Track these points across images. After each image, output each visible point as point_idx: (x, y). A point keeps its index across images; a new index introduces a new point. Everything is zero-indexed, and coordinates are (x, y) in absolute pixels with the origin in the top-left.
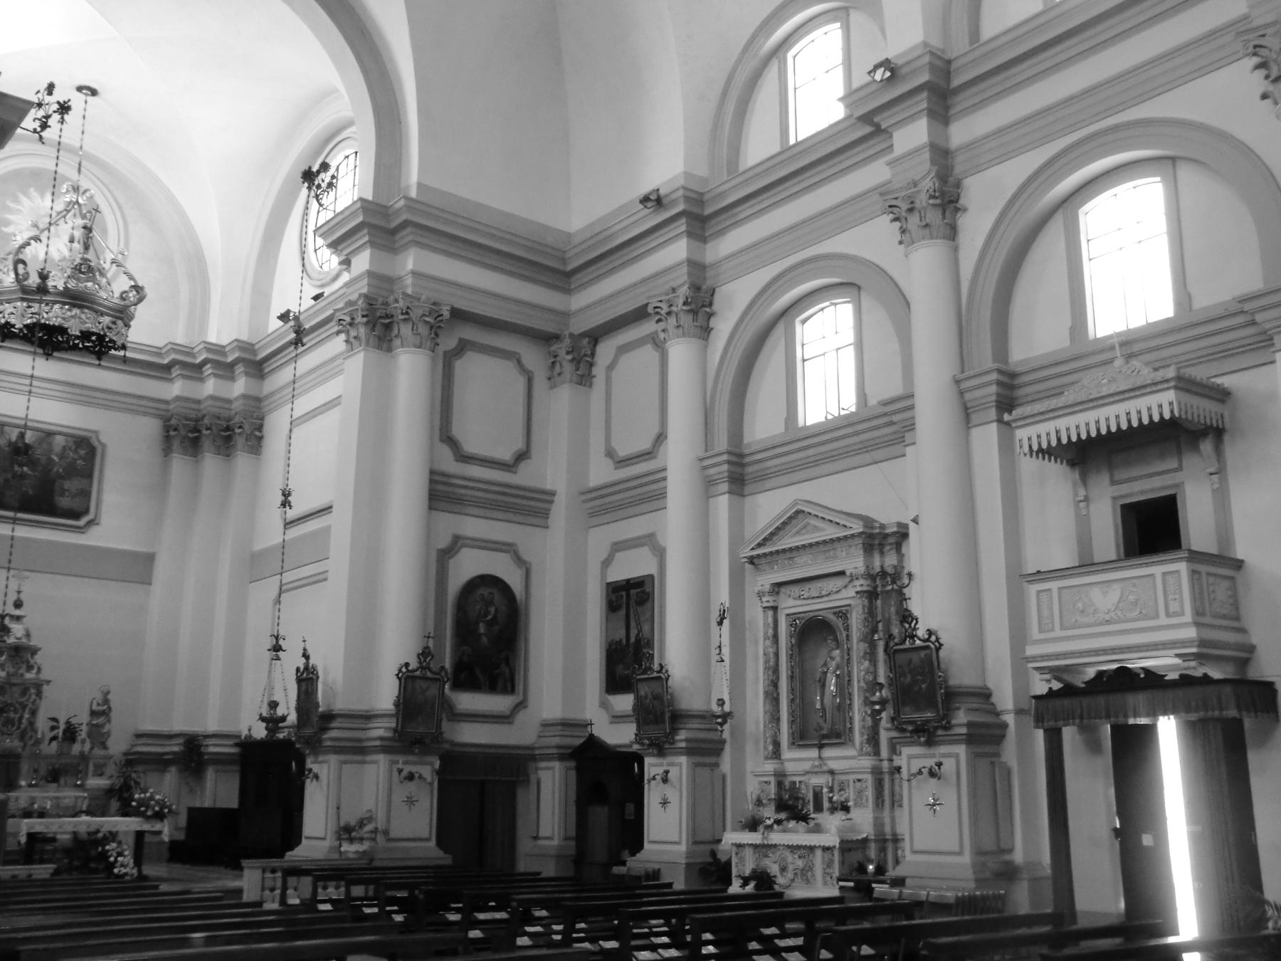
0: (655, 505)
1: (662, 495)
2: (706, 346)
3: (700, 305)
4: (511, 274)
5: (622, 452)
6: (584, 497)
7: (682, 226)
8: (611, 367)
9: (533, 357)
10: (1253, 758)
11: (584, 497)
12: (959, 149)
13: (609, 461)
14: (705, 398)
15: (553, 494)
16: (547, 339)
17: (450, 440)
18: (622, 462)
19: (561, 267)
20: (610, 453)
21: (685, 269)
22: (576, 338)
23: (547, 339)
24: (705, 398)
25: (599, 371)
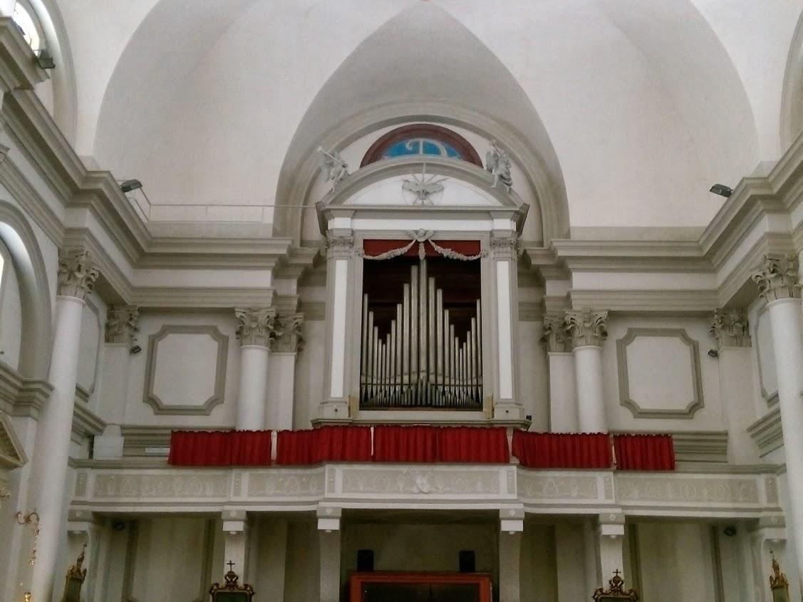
2: (574, 356)
7: (760, 206)
9: (698, 333)
17: (628, 404)
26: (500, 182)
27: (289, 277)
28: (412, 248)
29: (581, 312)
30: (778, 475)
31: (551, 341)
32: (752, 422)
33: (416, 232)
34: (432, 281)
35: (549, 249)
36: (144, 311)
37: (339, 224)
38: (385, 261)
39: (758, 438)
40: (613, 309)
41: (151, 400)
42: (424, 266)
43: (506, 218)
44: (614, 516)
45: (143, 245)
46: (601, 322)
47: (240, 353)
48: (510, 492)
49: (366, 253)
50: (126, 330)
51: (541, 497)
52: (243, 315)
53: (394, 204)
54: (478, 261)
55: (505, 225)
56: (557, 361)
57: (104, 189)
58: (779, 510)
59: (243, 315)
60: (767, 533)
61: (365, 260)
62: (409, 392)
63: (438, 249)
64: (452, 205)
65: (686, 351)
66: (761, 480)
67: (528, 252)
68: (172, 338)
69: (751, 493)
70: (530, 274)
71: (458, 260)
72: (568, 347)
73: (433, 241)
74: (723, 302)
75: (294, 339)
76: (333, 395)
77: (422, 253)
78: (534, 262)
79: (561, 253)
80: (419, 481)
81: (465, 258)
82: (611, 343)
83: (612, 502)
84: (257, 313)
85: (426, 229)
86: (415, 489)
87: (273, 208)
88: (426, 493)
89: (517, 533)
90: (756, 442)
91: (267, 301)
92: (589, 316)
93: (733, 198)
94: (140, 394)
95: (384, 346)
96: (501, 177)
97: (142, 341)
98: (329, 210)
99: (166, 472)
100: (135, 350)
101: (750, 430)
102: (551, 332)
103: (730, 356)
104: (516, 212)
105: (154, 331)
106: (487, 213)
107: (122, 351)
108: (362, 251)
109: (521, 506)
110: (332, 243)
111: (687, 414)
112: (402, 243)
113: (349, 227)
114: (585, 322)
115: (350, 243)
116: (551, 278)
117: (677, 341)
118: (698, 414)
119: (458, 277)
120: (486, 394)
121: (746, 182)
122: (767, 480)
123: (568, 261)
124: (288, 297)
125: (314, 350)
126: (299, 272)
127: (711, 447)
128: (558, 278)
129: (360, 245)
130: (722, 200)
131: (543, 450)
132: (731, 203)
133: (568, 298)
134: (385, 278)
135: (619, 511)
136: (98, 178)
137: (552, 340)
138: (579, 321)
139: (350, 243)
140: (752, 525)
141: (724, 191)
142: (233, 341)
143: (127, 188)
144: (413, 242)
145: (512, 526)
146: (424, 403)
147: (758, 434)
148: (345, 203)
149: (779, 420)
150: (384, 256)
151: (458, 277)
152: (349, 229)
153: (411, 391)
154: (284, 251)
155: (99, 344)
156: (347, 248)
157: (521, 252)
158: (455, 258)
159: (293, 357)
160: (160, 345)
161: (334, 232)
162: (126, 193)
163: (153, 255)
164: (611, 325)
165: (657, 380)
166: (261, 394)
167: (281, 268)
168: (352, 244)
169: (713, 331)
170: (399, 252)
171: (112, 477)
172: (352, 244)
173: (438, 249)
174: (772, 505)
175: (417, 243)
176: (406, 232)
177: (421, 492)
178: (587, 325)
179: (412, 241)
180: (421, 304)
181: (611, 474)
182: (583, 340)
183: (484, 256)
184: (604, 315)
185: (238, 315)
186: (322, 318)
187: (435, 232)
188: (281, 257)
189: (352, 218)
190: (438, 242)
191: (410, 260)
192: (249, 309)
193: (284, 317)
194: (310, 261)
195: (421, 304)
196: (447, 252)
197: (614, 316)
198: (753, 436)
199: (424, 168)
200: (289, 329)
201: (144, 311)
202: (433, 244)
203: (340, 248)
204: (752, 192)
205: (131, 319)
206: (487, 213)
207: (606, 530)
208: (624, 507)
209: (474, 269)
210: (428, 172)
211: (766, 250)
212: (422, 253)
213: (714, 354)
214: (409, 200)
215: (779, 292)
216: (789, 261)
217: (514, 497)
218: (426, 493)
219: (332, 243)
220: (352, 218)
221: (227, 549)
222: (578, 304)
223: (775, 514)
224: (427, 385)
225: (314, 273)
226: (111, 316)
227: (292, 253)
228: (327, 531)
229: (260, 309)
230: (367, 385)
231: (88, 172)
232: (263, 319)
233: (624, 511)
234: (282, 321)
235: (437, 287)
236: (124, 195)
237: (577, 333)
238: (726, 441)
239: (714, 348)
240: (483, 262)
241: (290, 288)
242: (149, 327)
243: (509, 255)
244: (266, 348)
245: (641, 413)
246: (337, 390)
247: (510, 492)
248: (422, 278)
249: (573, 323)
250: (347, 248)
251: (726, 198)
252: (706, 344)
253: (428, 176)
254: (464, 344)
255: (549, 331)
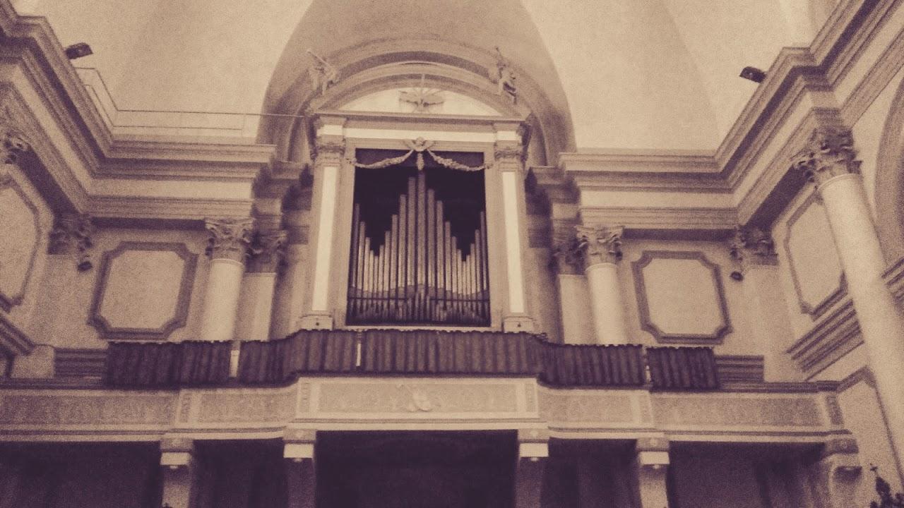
0: (855, 341)
1: (856, 330)
2: (586, 278)
3: (839, 145)
4: (679, 190)
5: (815, 303)
6: (793, 354)
7: (801, 81)
8: (787, 240)
9: (719, 256)
10: (716, 149)
11: (793, 354)
12: (666, 451)
13: (808, 316)
14: (870, 213)
15: (761, 359)
16: (721, 237)
18: (816, 313)
19: (713, 170)
20: (805, 309)
21: (813, 119)
22: (746, 230)
23: (721, 237)
24: (867, 205)
25: (780, 249)
26: (505, 92)
27: (274, 196)
28: (410, 157)
29: (593, 229)
30: (839, 392)
31: (560, 264)
32: (790, 344)
33: (414, 142)
34: (431, 195)
35: (556, 168)
36: (104, 224)
37: (329, 131)
38: (380, 170)
39: (801, 359)
40: (628, 226)
41: (97, 322)
42: (422, 178)
43: (511, 130)
44: (656, 442)
45: (105, 151)
46: (617, 240)
47: (208, 267)
48: (530, 409)
49: (359, 162)
50: (75, 242)
51: (565, 420)
52: (215, 227)
53: (387, 118)
54: (482, 172)
55: (511, 137)
56: (568, 283)
57: (37, 39)
58: (846, 432)
59: (215, 227)
60: (835, 461)
61: (357, 169)
62: (406, 307)
63: (440, 160)
64: (456, 119)
65: (706, 274)
66: (820, 398)
67: (534, 171)
68: (130, 256)
69: (811, 414)
70: (537, 199)
71: (460, 171)
72: (579, 267)
73: (432, 152)
74: (744, 221)
75: (275, 259)
76: (315, 308)
77: (420, 164)
78: (541, 182)
79: (569, 168)
80: (416, 396)
81: (468, 169)
82: (626, 263)
83: (650, 425)
84: (231, 225)
85: (426, 139)
86: (411, 407)
87: (259, 117)
88: (426, 411)
89: (541, 459)
90: (800, 363)
91: (244, 213)
92: (603, 232)
93: (766, 82)
94: (84, 314)
95: (376, 260)
96: (506, 85)
97: (95, 256)
98: (317, 116)
99: (98, 393)
100: (84, 267)
101: (789, 351)
102: (559, 253)
103: (755, 275)
104: (522, 124)
105: (111, 248)
106: (489, 124)
107: (69, 265)
108: (354, 159)
109: (661, 435)
110: (321, 148)
111: (715, 339)
112: (402, 153)
113: (341, 134)
114: (598, 239)
115: (341, 150)
116: (558, 201)
117: (695, 264)
118: (726, 339)
119: (458, 193)
120: (495, 306)
121: (788, 52)
122: (828, 399)
123: (577, 179)
124: (269, 216)
125: (298, 275)
126: (284, 189)
127: (745, 373)
128: (564, 201)
129: (351, 154)
130: (752, 86)
131: (560, 363)
132: (763, 89)
133: (578, 219)
134: (382, 190)
135: (661, 435)
136: (33, 25)
137: (562, 262)
138: (592, 239)
139: (341, 150)
140: (815, 453)
141: (753, 74)
142: (202, 258)
143: (73, 52)
144: (411, 153)
145: (534, 451)
146: (421, 367)
147: (801, 353)
148: (340, 109)
149: (853, 313)
150: (379, 164)
151: (458, 193)
152: (340, 136)
153: (408, 307)
154: (266, 160)
155: (34, 254)
156: (338, 155)
157: (527, 168)
158: (457, 168)
159: (273, 278)
160: (116, 263)
161: (323, 138)
162: (73, 61)
163: (118, 161)
164: (629, 242)
165: (680, 300)
166: (227, 305)
167: (263, 186)
168: (343, 151)
169: (734, 253)
170: (396, 160)
171: (24, 399)
172: (343, 151)
173: (440, 160)
174: (838, 428)
175: (415, 153)
176: (404, 142)
177: (421, 410)
178: (603, 241)
179: (408, 151)
180: (418, 209)
181: (646, 393)
182: (598, 258)
183: (488, 168)
184: (619, 232)
185: (209, 227)
186: (306, 242)
187: (435, 142)
188: (263, 167)
189: (344, 127)
190: (438, 153)
191: (407, 170)
192: (222, 221)
193: (263, 236)
194: (296, 177)
195: (418, 209)
196: (447, 162)
197: (631, 235)
198: (794, 358)
199: (423, 80)
200: (270, 248)
201: (104, 224)
202: (432, 154)
203: (329, 155)
204: (794, 63)
205: (82, 230)
206: (489, 124)
207: (646, 458)
208: (666, 432)
209: (477, 181)
210: (427, 85)
211: (814, 123)
212: (420, 164)
213: (737, 277)
214: (407, 110)
215: (837, 168)
216: (841, 136)
217: (535, 415)
218: (426, 411)
219: (321, 148)
220: (344, 127)
221: (166, 490)
222: (588, 220)
223: (843, 437)
224: (425, 300)
225: (299, 193)
226: (58, 224)
227: (277, 166)
228: (296, 460)
229: (235, 221)
230: (356, 299)
231: (19, 17)
232: (237, 231)
233: (668, 436)
234: (263, 240)
235: (436, 199)
236: (69, 62)
237: (590, 250)
238: (762, 367)
239: (738, 270)
240: (488, 174)
241: (276, 207)
242: (107, 241)
243: (515, 165)
244: (239, 263)
245: (665, 338)
246: (320, 302)
247: (530, 409)
248: (420, 195)
249: (585, 241)
250: (338, 155)
251: (757, 84)
252: (727, 268)
253: (426, 90)
254: (468, 257)
255: (558, 253)
